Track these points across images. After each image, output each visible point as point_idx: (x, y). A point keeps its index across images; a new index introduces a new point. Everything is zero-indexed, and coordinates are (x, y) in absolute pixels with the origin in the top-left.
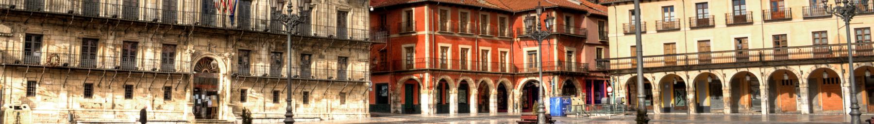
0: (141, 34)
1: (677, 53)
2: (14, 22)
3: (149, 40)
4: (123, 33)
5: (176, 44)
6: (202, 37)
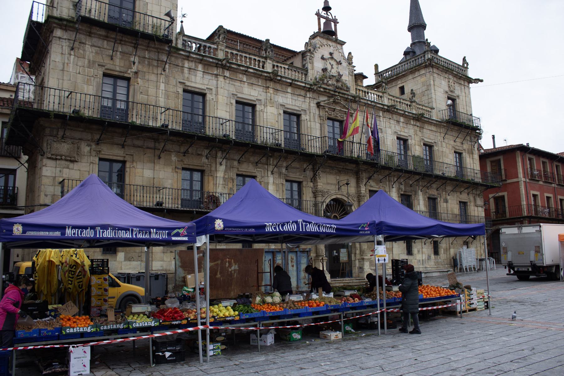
0: (259, 165)
1: (35, 204)
2: (81, 139)
3: (270, 173)
4: (236, 163)
5: (301, 180)
6: (330, 173)
